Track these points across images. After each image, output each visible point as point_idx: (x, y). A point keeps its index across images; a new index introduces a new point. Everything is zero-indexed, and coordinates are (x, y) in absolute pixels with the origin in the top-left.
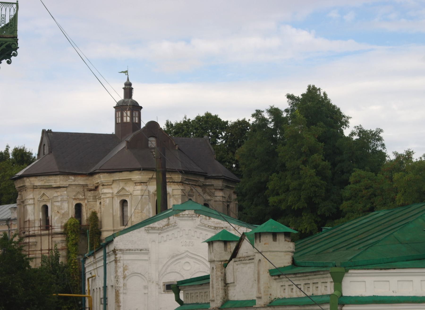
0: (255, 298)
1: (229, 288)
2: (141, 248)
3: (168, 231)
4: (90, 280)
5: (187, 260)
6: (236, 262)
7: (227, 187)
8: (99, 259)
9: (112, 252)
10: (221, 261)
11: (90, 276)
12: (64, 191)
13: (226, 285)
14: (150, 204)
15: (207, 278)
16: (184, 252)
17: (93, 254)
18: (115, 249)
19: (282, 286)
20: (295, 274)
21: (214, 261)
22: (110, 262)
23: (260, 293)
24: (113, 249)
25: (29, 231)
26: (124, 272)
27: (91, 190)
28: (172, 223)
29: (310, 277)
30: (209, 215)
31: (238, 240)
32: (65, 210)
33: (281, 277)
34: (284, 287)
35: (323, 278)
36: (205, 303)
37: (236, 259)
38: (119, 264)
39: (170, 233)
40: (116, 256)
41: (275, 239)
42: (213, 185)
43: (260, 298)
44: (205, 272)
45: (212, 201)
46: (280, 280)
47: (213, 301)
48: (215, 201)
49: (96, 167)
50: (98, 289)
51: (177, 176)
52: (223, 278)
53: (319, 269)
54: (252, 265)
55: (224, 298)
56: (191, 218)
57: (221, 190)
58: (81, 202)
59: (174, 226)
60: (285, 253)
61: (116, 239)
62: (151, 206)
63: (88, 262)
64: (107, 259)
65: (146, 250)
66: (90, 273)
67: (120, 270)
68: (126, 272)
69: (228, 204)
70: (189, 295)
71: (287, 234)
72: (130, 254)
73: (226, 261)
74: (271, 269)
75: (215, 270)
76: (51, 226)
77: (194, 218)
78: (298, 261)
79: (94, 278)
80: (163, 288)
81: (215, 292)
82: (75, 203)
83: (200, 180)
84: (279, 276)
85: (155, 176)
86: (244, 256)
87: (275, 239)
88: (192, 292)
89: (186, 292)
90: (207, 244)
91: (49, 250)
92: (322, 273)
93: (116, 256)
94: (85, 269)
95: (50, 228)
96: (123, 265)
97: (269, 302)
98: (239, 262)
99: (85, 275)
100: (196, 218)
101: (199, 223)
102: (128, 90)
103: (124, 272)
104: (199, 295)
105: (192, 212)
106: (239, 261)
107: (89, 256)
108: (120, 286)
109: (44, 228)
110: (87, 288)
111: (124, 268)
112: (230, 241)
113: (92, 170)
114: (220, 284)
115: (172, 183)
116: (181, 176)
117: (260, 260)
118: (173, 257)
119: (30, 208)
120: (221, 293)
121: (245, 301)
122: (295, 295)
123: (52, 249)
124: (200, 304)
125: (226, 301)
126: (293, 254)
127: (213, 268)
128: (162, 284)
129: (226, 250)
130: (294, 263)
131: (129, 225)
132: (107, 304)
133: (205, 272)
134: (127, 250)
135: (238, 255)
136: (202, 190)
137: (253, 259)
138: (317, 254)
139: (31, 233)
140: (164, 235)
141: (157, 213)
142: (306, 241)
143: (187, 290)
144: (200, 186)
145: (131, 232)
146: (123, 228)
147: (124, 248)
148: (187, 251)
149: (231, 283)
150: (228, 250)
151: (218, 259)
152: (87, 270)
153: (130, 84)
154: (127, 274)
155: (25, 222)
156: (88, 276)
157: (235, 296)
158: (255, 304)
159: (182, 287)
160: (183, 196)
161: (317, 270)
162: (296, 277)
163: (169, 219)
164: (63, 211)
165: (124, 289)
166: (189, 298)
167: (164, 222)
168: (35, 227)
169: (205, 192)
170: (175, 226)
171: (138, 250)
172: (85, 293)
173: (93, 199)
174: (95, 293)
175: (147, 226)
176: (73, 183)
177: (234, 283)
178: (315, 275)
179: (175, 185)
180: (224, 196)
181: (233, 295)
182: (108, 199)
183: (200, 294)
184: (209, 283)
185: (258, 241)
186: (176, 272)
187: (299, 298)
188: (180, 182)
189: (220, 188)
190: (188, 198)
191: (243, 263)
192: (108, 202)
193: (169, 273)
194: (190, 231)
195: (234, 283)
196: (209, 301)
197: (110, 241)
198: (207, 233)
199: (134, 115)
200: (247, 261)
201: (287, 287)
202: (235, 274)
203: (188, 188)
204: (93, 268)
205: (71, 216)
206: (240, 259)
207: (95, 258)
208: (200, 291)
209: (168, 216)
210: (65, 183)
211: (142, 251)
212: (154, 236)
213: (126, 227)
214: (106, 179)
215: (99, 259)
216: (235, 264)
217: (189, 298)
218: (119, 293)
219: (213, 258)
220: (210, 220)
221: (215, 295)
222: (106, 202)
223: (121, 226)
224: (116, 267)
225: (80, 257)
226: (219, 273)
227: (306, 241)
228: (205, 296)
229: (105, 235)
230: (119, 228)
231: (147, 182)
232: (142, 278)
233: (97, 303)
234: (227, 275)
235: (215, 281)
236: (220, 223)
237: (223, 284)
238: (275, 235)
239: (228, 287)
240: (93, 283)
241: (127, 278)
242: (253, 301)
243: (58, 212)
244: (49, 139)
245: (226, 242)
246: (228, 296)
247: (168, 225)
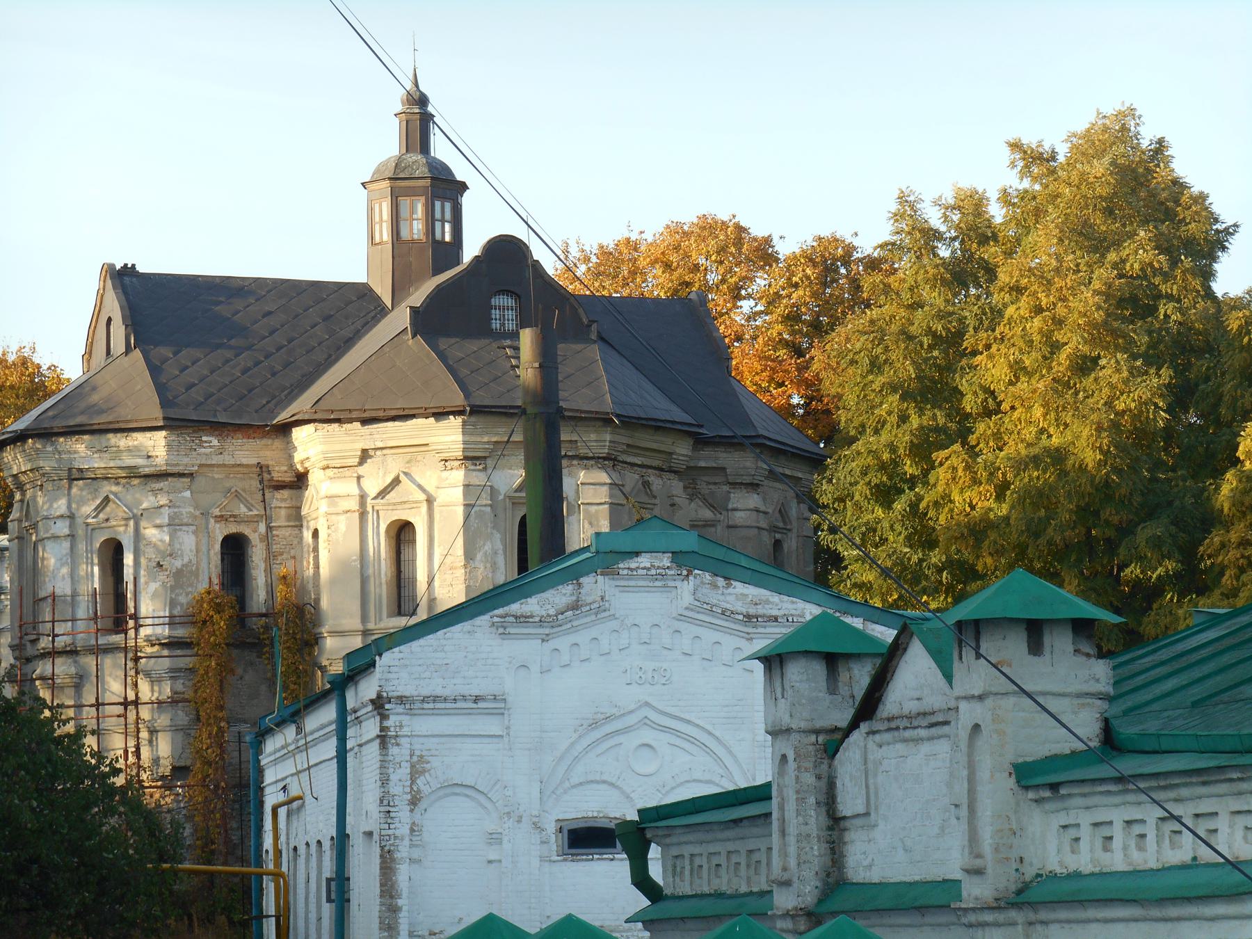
0: (958, 875)
1: (848, 836)
2: (476, 692)
3: (575, 629)
4: (282, 812)
5: (647, 736)
6: (877, 737)
7: (772, 475)
8: (316, 735)
9: (370, 708)
10: (817, 732)
11: (281, 797)
12: (185, 489)
13: (835, 823)
14: (498, 536)
15: (761, 794)
16: (633, 707)
17: (295, 717)
18: (379, 696)
19: (1065, 827)
20: (1120, 779)
21: (788, 731)
22: (361, 745)
23: (979, 856)
24: (374, 696)
25: (55, 636)
26: (413, 781)
27: (280, 486)
28: (589, 600)
29: (1184, 792)
30: (725, 570)
31: (884, 651)
32: (186, 560)
33: (1063, 791)
34: (1072, 833)
35: (1240, 794)
36: (751, 893)
37: (876, 725)
38: (393, 750)
39: (583, 637)
40: (386, 724)
41: (1035, 647)
42: (724, 469)
43: (978, 872)
44: (708, 782)
45: (719, 528)
46: (1059, 805)
47: (787, 884)
48: (729, 527)
49: (302, 404)
50: (313, 847)
51: (593, 436)
52: (822, 798)
53: (1222, 760)
54: (943, 747)
55: (828, 875)
56: (658, 584)
57: (753, 486)
58: (246, 530)
59: (600, 610)
60: (1076, 701)
61: (386, 660)
62: (499, 546)
63: (272, 745)
64: (350, 733)
65: (495, 698)
66: (281, 785)
67: (399, 775)
68: (420, 782)
69: (778, 536)
70: (687, 862)
71: (1081, 627)
72: (435, 713)
73: (836, 729)
74: (1020, 760)
75: (792, 765)
76: (135, 617)
77: (671, 584)
78: (1126, 730)
79: (295, 805)
80: (554, 842)
81: (792, 849)
82: (220, 532)
83: (678, 450)
84: (1054, 787)
85: (518, 437)
86: (906, 711)
87: (1035, 647)
88: (696, 849)
89: (675, 851)
90: (759, 667)
91: (125, 704)
92: (1235, 776)
93: (386, 724)
94: (260, 771)
95: (131, 623)
96: (411, 756)
97: (1013, 888)
98: (887, 737)
99: (260, 790)
100: (678, 584)
101: (687, 599)
102: (419, 120)
103: (413, 781)
104: (724, 865)
105: (666, 561)
106: (889, 729)
107: (281, 723)
108: (398, 833)
109: (109, 623)
110: (268, 842)
111: (412, 766)
112: (848, 657)
113: (283, 416)
114: (812, 821)
115: (575, 462)
116: (608, 437)
117: (977, 727)
118: (594, 725)
119: (52, 557)
120: (816, 851)
121: (916, 883)
122: (1117, 861)
123: (136, 703)
124: (731, 897)
125: (835, 880)
126: (1103, 705)
127: (784, 757)
128: (551, 828)
129: (832, 689)
130: (1110, 741)
131: (422, 615)
132: (349, 901)
133: (708, 782)
134: (424, 700)
135: (881, 707)
136: (685, 487)
137: (946, 723)
138: (1195, 704)
139: (61, 642)
140: (563, 643)
141: (523, 566)
142: (1133, 660)
143: (679, 844)
144: (675, 472)
145: (441, 633)
146: (403, 622)
147: (415, 693)
148: (647, 704)
149: (858, 816)
150: (843, 690)
151: (803, 725)
152: (269, 777)
153: (422, 101)
154: (426, 790)
155: (38, 601)
156: (272, 798)
157: (870, 866)
158: (959, 898)
159: (660, 833)
160: (614, 507)
161: (1212, 763)
162: (1127, 791)
163: (579, 585)
164: (178, 564)
165: (411, 846)
166: (687, 873)
167: (559, 596)
168: (74, 620)
169: (693, 493)
170: (601, 608)
171: (464, 698)
172: (259, 862)
173: (289, 518)
174: (301, 861)
175: (500, 611)
176: (216, 460)
177: (867, 814)
178: (1204, 783)
179: (586, 468)
180: (763, 508)
181: (865, 863)
182: (343, 518)
183: (728, 858)
184: (768, 815)
185: (968, 654)
186: (604, 782)
187: (1102, 874)
188: (605, 459)
189: (747, 480)
190: (633, 512)
191: (905, 741)
192: (342, 527)
193: (581, 784)
194: (655, 630)
195: (867, 814)
196: (765, 888)
197: (360, 665)
198: (717, 636)
199: (438, 215)
200: (922, 733)
201: (1085, 832)
202: (871, 781)
203: (631, 479)
204: (294, 767)
205: (205, 585)
206: (893, 725)
207: (299, 730)
208: (731, 846)
209: (574, 575)
210: (186, 460)
211: (481, 705)
212: (528, 648)
213: (413, 621)
214: (338, 447)
215: (316, 735)
216: (871, 742)
217: (687, 873)
218: (393, 860)
219: (786, 720)
220: (730, 590)
221: (792, 863)
222: (336, 530)
223: (390, 616)
224: (383, 765)
225: (244, 728)
226: (809, 779)
227: (1133, 660)
228: (748, 866)
229: (334, 650)
230: (382, 625)
231: (485, 458)
232: (481, 805)
233: (307, 898)
234: (839, 784)
235: (791, 807)
236: (768, 602)
237: (824, 820)
238: (1035, 631)
239: (845, 829)
240: (295, 824)
241: (423, 805)
242: (951, 886)
243: (159, 565)
244: (128, 300)
245: (832, 660)
246: (844, 867)
247: (575, 606)
